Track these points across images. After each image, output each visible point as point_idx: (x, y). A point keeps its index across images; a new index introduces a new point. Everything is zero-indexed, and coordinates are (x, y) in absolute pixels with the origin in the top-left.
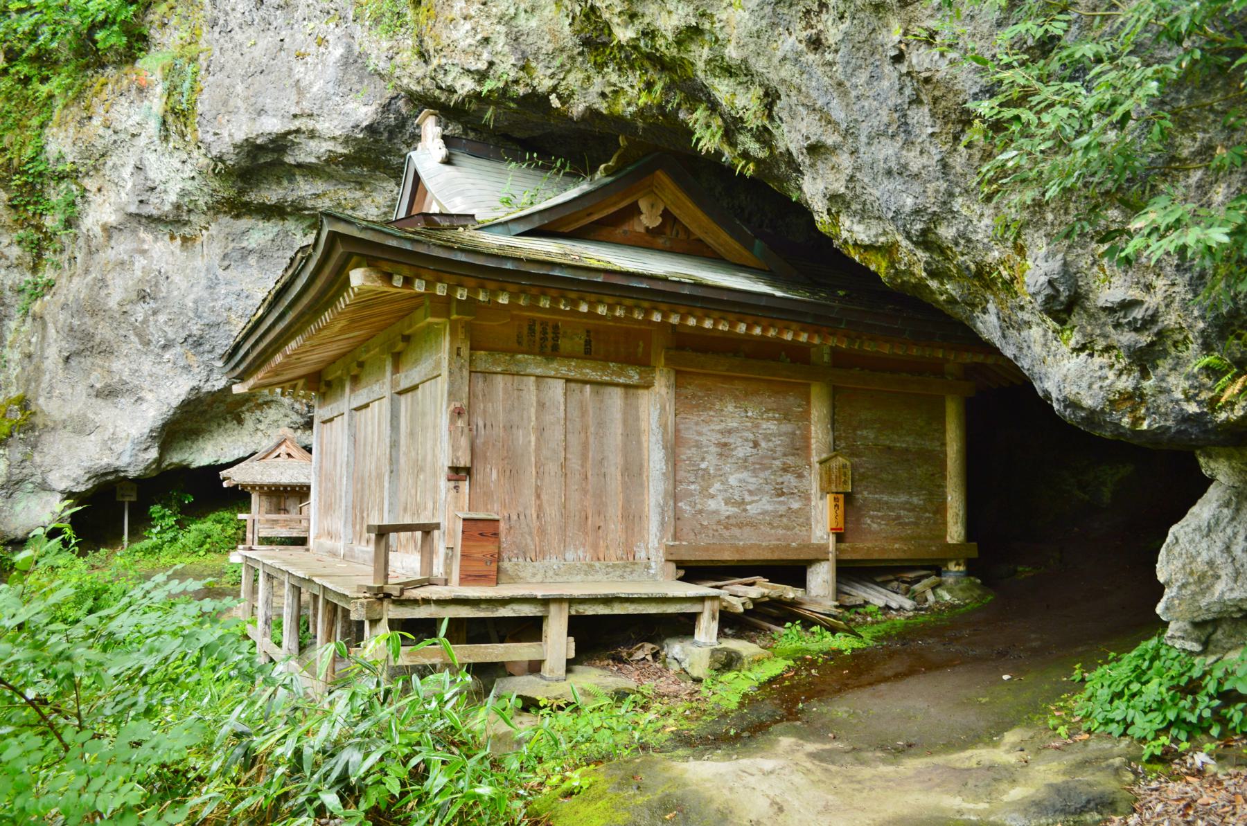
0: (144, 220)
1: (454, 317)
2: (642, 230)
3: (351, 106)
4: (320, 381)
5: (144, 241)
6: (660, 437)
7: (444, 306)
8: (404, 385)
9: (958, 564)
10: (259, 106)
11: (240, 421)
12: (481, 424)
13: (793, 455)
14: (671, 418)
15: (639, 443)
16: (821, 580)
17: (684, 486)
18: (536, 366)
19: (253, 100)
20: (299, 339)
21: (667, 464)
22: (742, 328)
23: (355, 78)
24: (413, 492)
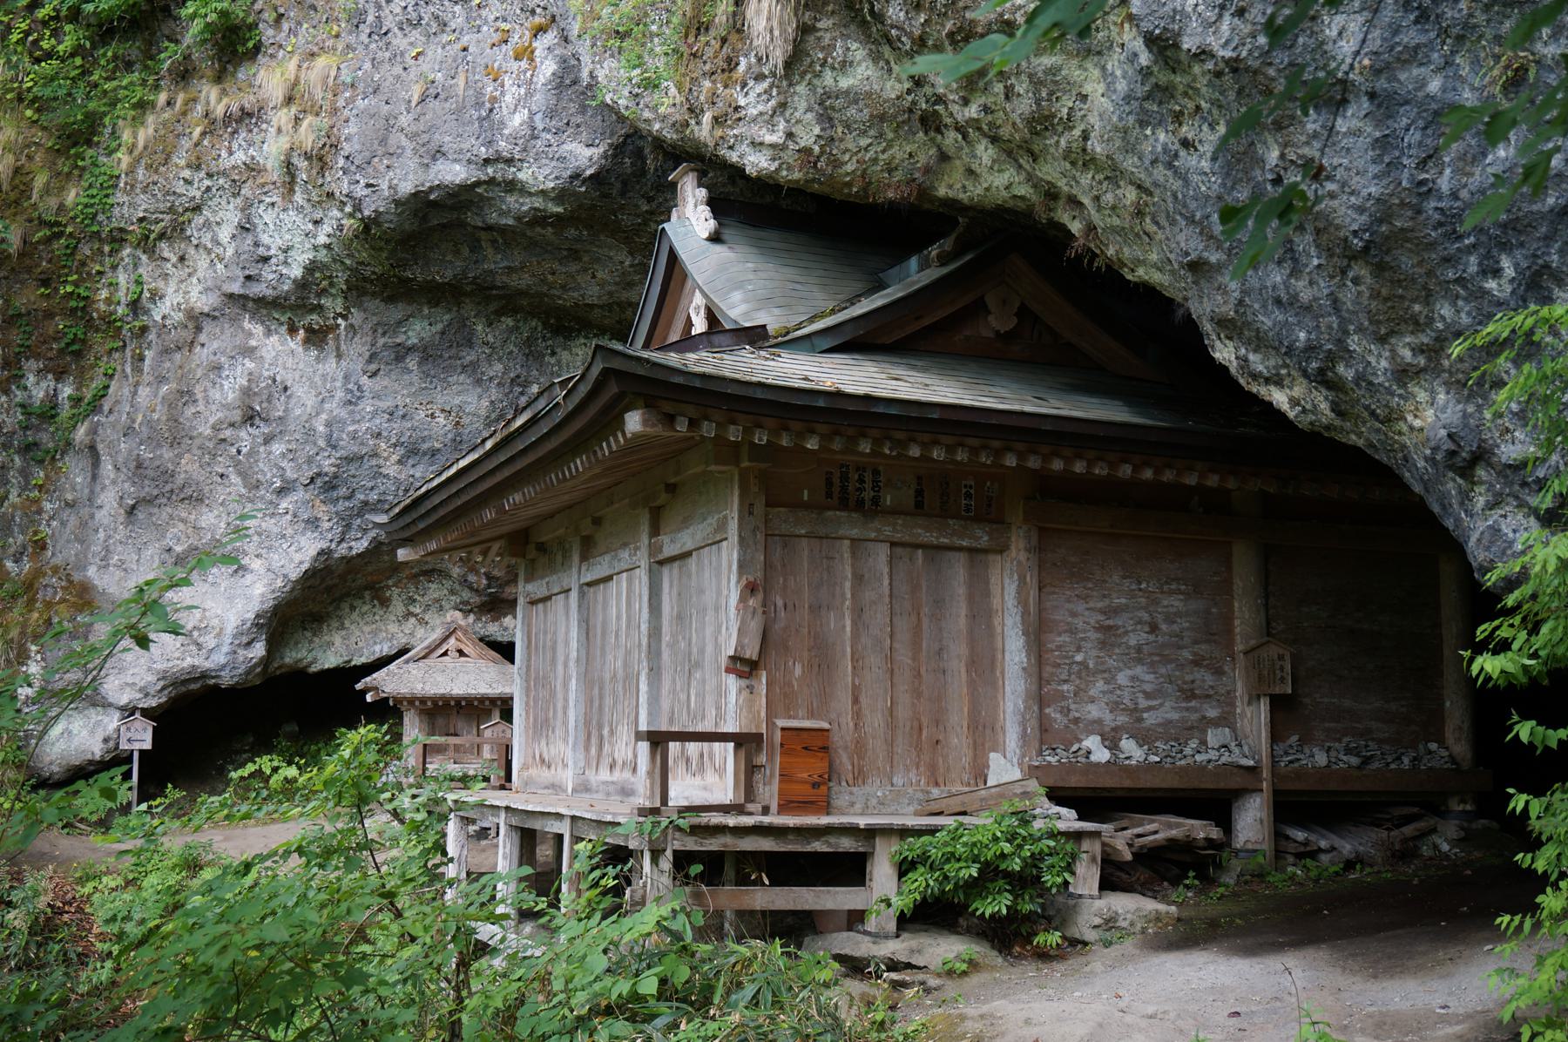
0: (250, 304)
1: (745, 464)
2: (991, 335)
3: (568, 147)
4: (527, 543)
5: (250, 334)
6: (1018, 618)
7: (728, 453)
8: (669, 550)
9: (1463, 801)
10: (433, 146)
11: (385, 603)
12: (780, 603)
13: (1208, 641)
14: (1033, 593)
15: (990, 627)
16: (1251, 822)
17: (1054, 686)
18: (850, 527)
19: (425, 137)
20: (529, 491)
21: (1028, 655)
22: (1126, 471)
23: (573, 107)
24: (683, 697)
